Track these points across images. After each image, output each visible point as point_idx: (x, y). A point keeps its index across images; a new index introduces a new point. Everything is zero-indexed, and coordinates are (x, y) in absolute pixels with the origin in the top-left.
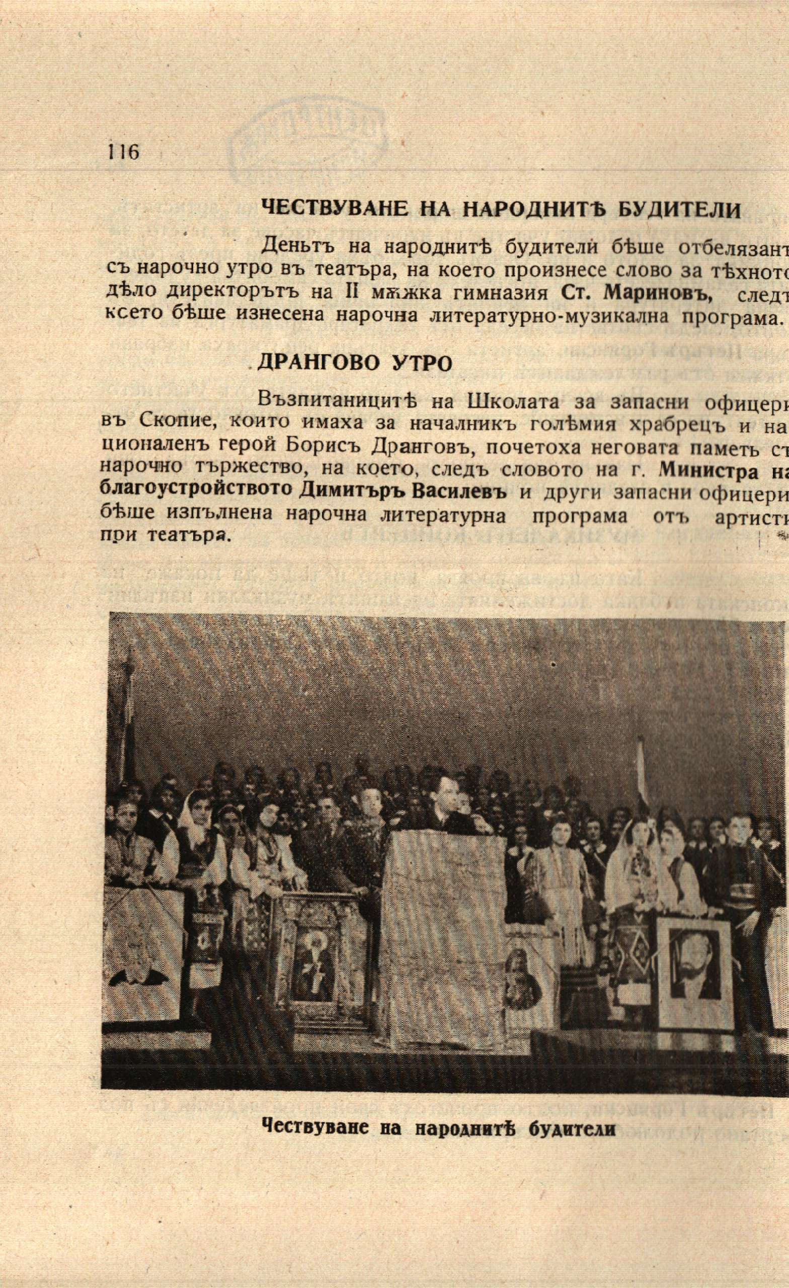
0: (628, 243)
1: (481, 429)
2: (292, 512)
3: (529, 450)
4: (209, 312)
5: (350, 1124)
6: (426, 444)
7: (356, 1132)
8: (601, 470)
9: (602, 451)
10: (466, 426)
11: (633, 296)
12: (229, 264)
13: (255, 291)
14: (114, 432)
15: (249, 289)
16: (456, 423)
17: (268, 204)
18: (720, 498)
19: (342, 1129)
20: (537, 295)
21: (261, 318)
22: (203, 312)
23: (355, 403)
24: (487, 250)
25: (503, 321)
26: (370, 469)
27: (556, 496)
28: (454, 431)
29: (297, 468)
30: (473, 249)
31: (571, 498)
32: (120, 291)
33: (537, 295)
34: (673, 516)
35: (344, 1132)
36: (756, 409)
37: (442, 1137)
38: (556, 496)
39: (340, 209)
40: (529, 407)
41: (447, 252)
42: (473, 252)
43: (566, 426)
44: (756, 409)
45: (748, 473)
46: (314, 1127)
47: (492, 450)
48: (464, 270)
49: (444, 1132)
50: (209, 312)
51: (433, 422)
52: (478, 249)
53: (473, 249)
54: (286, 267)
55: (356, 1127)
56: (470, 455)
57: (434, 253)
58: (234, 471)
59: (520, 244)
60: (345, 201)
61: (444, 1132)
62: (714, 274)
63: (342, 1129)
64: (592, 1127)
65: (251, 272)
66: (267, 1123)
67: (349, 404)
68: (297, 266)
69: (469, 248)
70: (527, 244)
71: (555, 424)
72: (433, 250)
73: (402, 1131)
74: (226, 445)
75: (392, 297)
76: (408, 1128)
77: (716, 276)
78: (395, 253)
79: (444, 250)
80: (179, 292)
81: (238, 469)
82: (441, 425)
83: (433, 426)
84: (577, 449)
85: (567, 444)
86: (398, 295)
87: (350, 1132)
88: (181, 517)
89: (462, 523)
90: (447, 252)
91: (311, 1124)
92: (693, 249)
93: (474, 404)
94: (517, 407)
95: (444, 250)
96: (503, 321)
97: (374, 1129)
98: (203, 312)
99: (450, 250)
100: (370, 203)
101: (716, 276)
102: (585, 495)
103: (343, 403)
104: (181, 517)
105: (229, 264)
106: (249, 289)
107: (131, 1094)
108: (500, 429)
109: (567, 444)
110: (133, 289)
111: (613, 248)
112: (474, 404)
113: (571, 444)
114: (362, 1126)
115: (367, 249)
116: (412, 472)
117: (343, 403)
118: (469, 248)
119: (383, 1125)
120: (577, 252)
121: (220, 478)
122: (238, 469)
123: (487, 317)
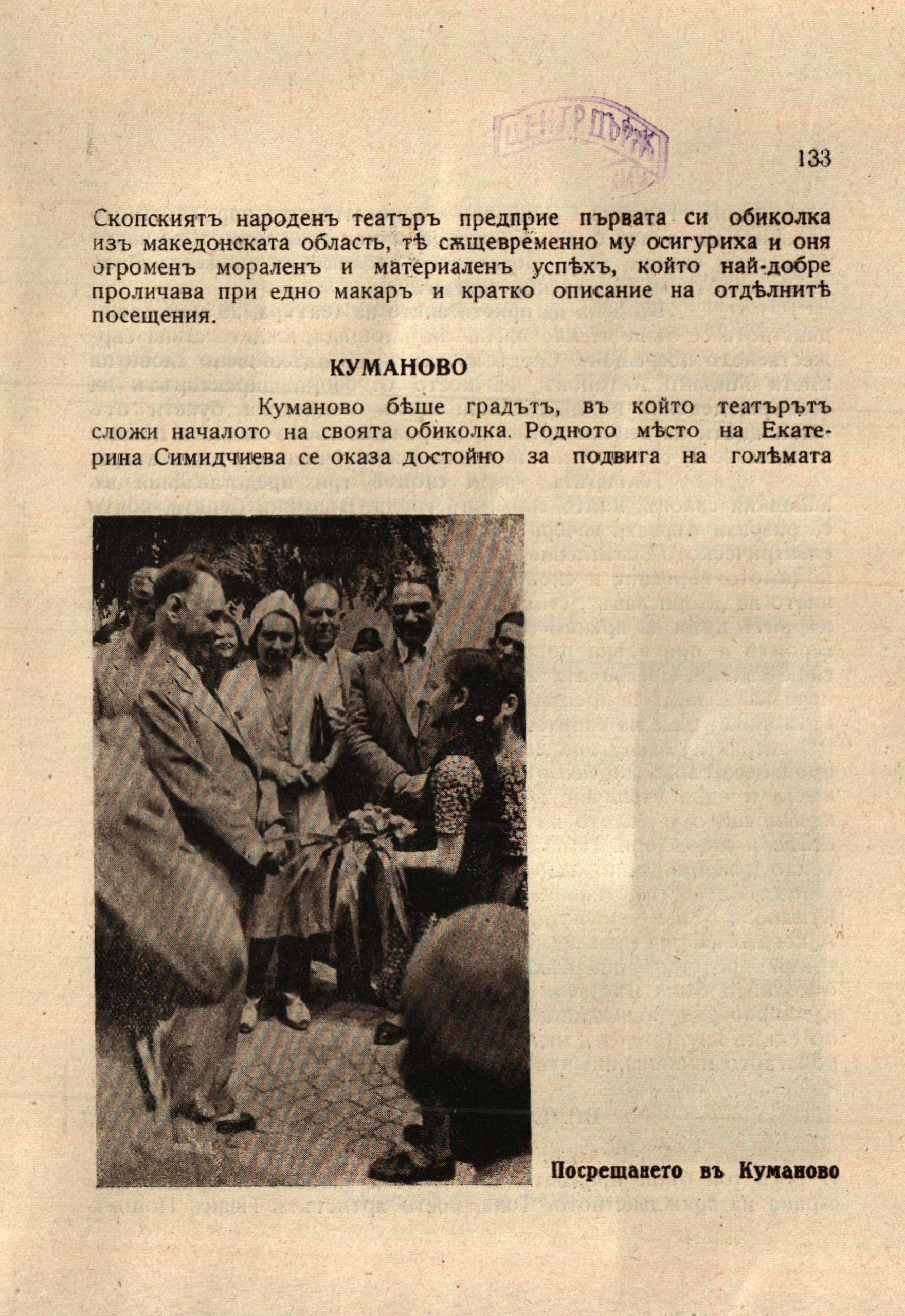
1: (795, 295)
2: (688, 454)
4: (427, 406)
5: (796, 1168)
6: (642, 453)
7: (802, 1177)
8: (290, 433)
9: (548, 221)
10: (779, 293)
16: (462, 266)
19: (634, 1173)
20: (184, 222)
22: (421, 407)
23: (792, 293)
26: (647, 408)
28: (221, 440)
33: (184, 222)
35: (636, 1176)
36: (156, 322)
37: (589, 1180)
39: (353, 369)
40: (352, 297)
43: (768, 458)
44: (156, 322)
45: (487, 292)
47: (98, 319)
50: (427, 406)
51: (196, 432)
58: (131, 438)
60: (358, 361)
63: (634, 1173)
65: (479, 412)
67: (124, 462)
71: (756, 456)
73: (707, 459)
74: (738, 458)
76: (692, 1170)
80: (566, 433)
81: (135, 436)
82: (205, 434)
83: (196, 434)
84: (753, 244)
85: (743, 238)
87: (797, 1176)
91: (708, 1168)
92: (594, 432)
93: (147, 320)
94: (134, 297)
98: (421, 407)
100: (391, 363)
102: (736, 460)
103: (313, 411)
109: (743, 238)
111: (389, 409)
112: (147, 320)
113: (791, 427)
117: (313, 411)
120: (104, 437)
122: (135, 436)
123: (490, 408)
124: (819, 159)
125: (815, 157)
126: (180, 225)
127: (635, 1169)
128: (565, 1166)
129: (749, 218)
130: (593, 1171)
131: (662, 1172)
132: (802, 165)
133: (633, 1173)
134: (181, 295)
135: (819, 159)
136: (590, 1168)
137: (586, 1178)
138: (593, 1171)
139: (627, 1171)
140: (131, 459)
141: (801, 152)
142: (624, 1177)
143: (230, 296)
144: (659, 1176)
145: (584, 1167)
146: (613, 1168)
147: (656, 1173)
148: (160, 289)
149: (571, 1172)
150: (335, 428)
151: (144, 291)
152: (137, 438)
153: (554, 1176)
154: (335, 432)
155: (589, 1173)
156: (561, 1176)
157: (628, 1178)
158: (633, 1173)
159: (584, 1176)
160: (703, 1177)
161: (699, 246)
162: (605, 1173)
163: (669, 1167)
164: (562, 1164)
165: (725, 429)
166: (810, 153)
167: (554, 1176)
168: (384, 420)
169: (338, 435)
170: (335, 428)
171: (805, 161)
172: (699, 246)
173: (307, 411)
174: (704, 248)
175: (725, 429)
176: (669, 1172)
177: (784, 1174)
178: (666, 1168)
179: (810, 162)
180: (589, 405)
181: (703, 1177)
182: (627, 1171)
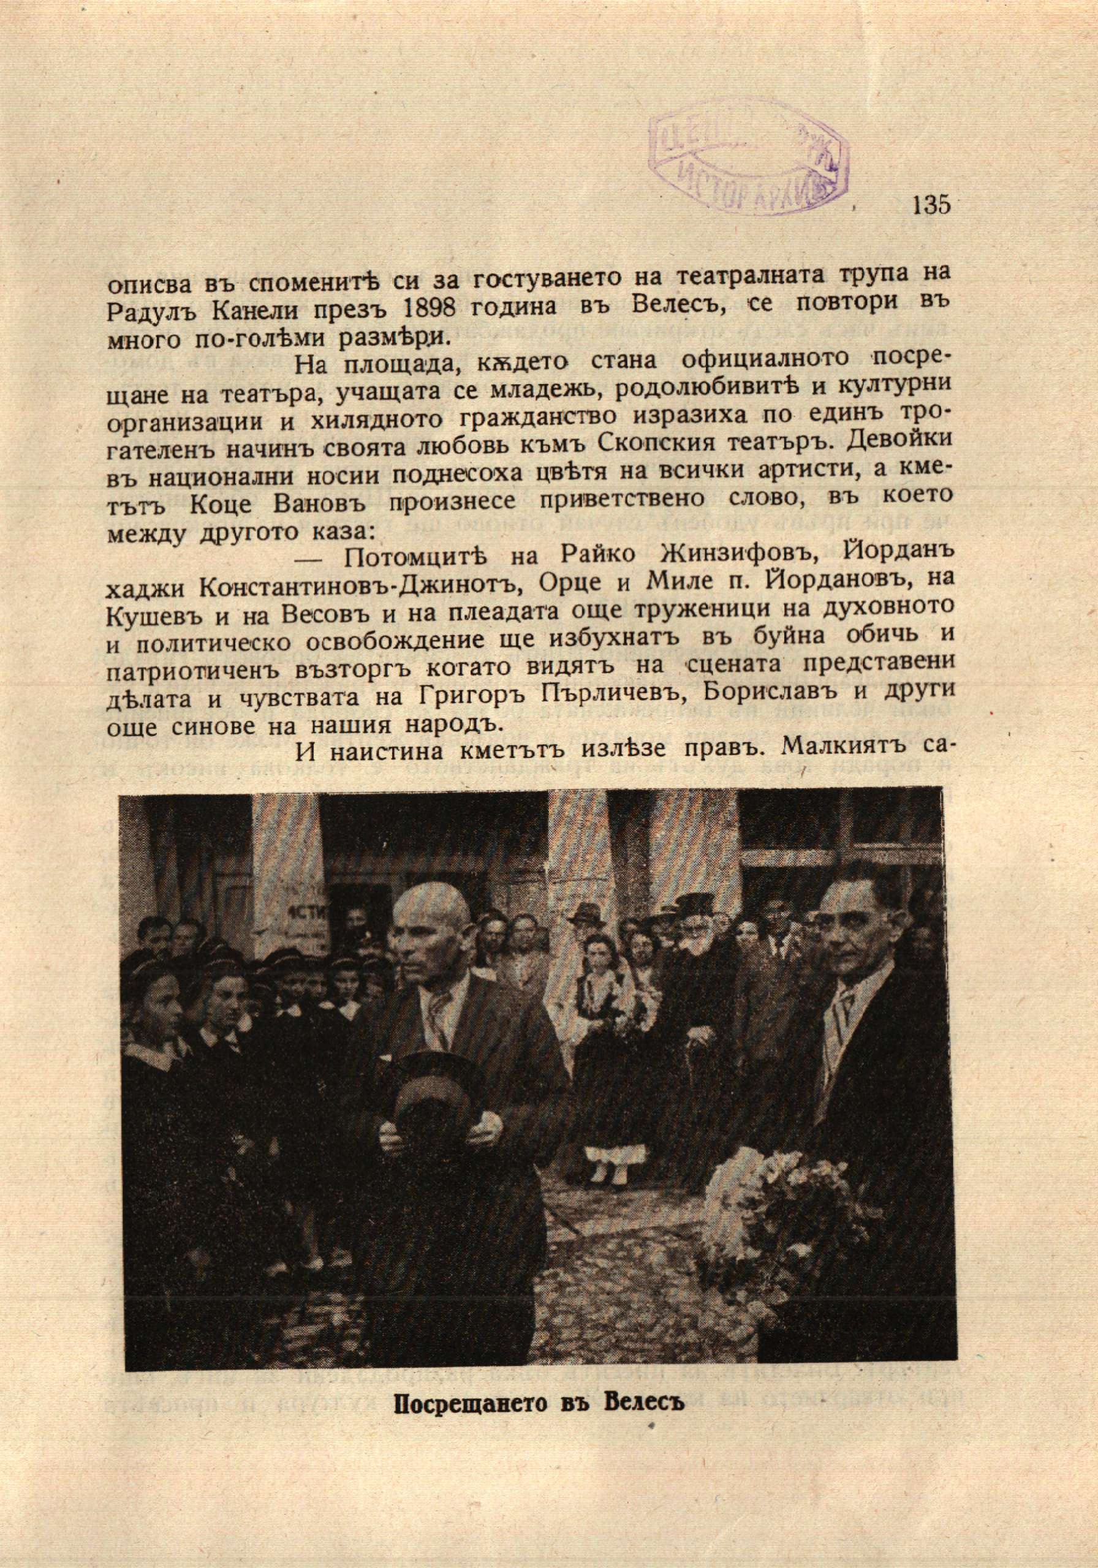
0: (630, 743)
3: (499, 754)
5: (500, 1400)
7: (507, 1410)
11: (433, 728)
12: (339, 389)
13: (501, 696)
14: (940, 564)
15: (493, 693)
17: (246, 698)
18: (756, 559)
20: (702, 445)
21: (467, 507)
24: (793, 389)
25: (887, 389)
27: (899, 693)
29: (791, 498)
30: (265, 397)
31: (918, 697)
32: (123, 703)
34: (594, 664)
35: (493, 1410)
37: (439, 1415)
38: (899, 693)
41: (389, 426)
42: (591, 671)
46: (805, 748)
48: (836, 662)
49: (442, 1408)
52: (471, 559)
53: (265, 397)
54: (113, 478)
55: (507, 1404)
56: (828, 448)
57: (819, 588)
59: (771, 633)
61: (442, 1408)
62: (638, 613)
64: (629, 1400)
66: (403, 1404)
68: (379, 582)
69: (459, 559)
70: (163, 309)
72: (818, 583)
75: (502, 369)
77: (113, 513)
78: (242, 458)
79: (385, 423)
81: (684, 613)
86: (509, 365)
87: (500, 1410)
88: (720, 559)
89: (898, 392)
90: (389, 426)
91: (571, 1399)
95: (385, 423)
96: (887, 389)
97: (555, 1404)
99: (392, 424)
101: (113, 513)
104: (720, 559)
105: (339, 389)
106: (493, 693)
107: (114, 1080)
108: (531, 451)
110: (140, 700)
114: (453, 1402)
115: (657, 278)
116: (795, 502)
118: (459, 559)
119: (564, 1399)
121: (916, 426)
122: (684, 613)
124: (936, 204)
125: (932, 204)
126: (373, 731)
127: (492, 1402)
128: (410, 1400)
129: (868, 635)
130: (442, 1405)
131: (524, 1405)
132: (917, 212)
133: (489, 1407)
134: (728, 752)
135: (936, 204)
136: (438, 1401)
137: (435, 1413)
138: (442, 1405)
139: (482, 1403)
140: (423, 614)
141: (917, 198)
142: (478, 1411)
143: (699, 751)
144: (520, 1409)
145: (431, 1401)
146: (465, 1401)
147: (518, 1406)
148: (894, 629)
149: (623, 1403)
150: (336, 639)
151: (180, 644)
152: (687, 615)
153: (398, 1411)
154: (336, 643)
155: (438, 1407)
156: (406, 1411)
157: (484, 1413)
158: (489, 1407)
159: (433, 1410)
160: (565, 1409)
161: (901, 389)
162: (456, 1407)
163: (533, 1399)
164: (406, 1396)
165: (789, 606)
166: (927, 198)
167: (398, 1411)
168: (739, 456)
169: (340, 646)
170: (336, 639)
171: (922, 209)
172: (901, 389)
173: (253, 398)
174: (906, 389)
175: (789, 606)
176: (533, 1405)
177: (485, 1407)
178: (529, 1400)
179: (926, 209)
180: (113, 478)
181: (565, 1409)
182: (482, 1403)
